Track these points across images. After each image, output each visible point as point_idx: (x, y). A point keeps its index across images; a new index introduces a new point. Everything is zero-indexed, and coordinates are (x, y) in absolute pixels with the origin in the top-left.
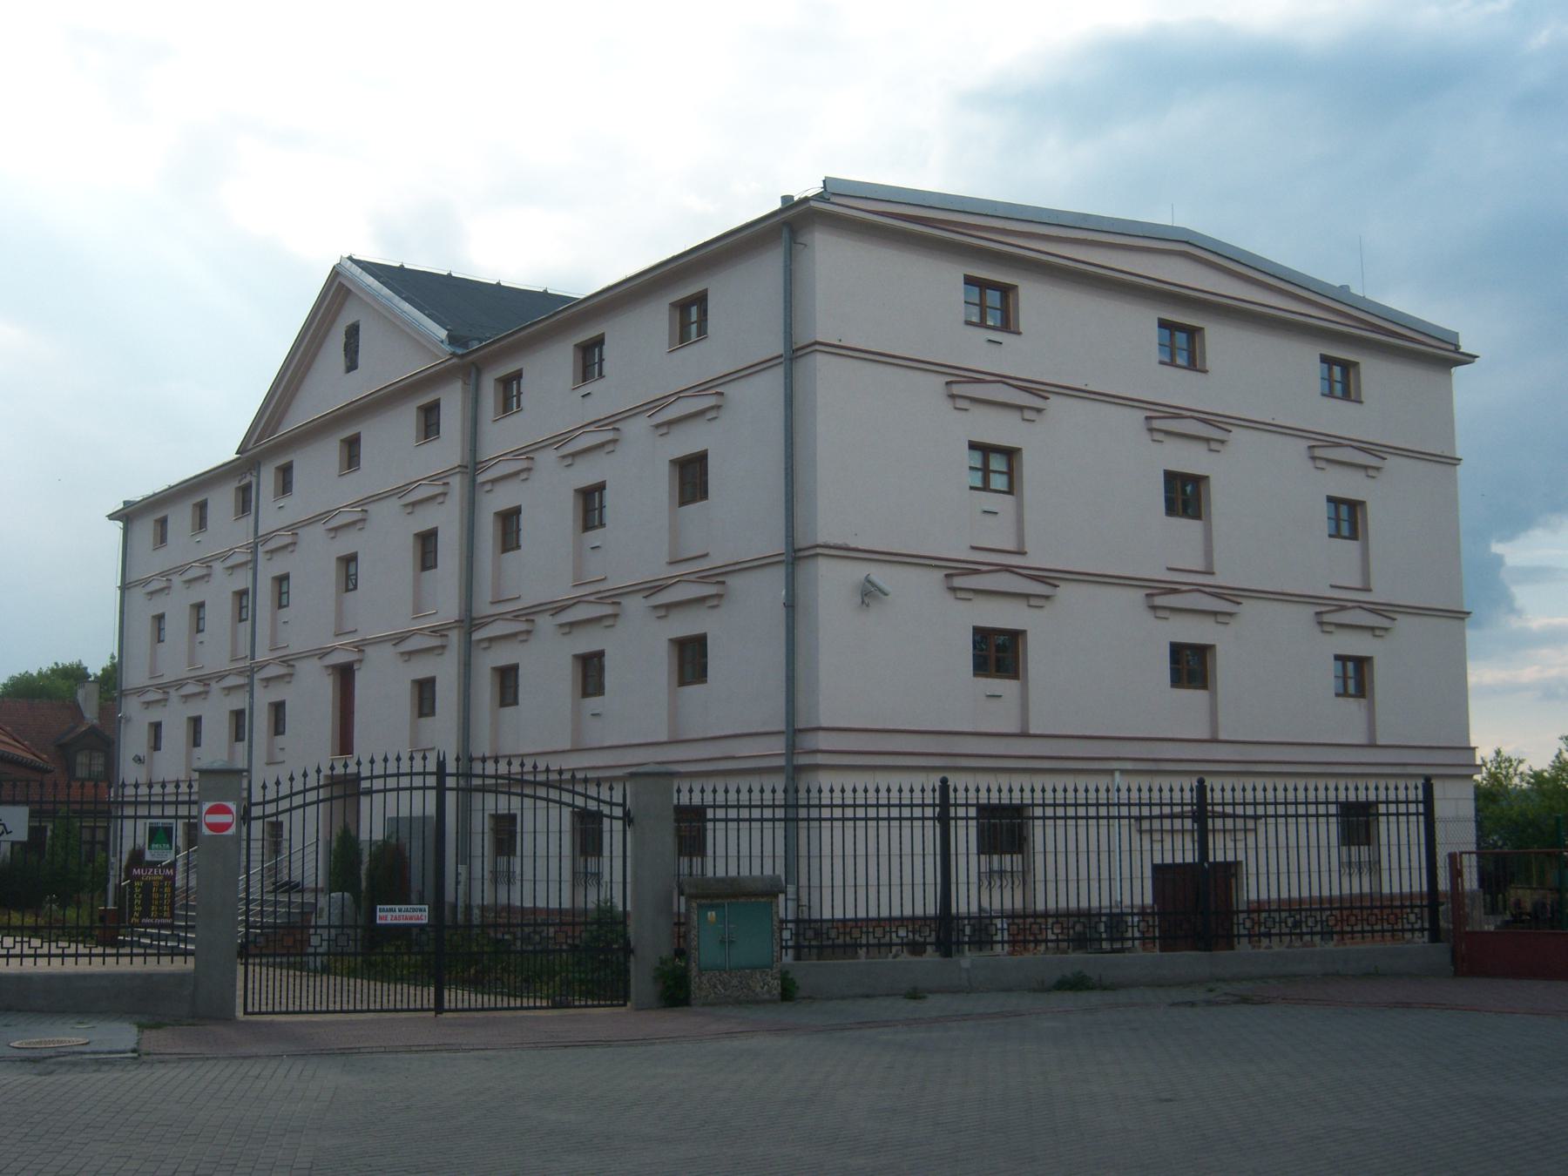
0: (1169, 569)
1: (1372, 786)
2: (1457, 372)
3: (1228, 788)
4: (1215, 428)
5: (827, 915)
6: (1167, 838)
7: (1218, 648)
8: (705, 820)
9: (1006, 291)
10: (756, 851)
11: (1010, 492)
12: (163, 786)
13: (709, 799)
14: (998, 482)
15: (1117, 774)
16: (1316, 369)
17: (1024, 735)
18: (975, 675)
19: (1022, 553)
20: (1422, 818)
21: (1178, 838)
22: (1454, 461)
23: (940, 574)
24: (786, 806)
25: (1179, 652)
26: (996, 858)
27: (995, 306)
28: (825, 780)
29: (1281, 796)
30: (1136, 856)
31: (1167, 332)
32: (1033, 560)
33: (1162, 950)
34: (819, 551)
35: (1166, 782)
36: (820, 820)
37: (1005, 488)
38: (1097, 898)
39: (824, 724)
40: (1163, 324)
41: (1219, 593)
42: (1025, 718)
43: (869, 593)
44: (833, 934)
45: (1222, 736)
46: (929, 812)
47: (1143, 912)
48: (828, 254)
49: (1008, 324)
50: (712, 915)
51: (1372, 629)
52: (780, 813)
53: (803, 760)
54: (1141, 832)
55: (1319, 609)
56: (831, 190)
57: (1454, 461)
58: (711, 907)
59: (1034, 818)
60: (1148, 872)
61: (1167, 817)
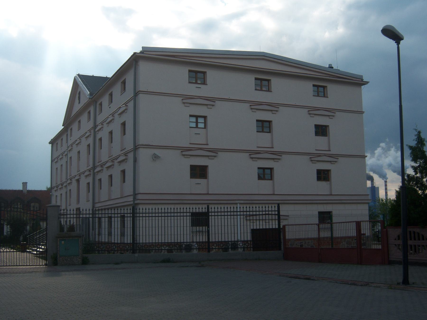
0: (190, 144)
1: (261, 207)
2: (363, 87)
3: (154, 209)
4: (274, 107)
5: (141, 242)
6: (271, 221)
7: (275, 169)
8: (209, 216)
9: (324, 87)
10: (147, 226)
11: (205, 128)
12: (64, 210)
13: (126, 212)
14: (201, 125)
15: (238, 204)
16: (311, 88)
17: (208, 194)
18: (191, 178)
19: (207, 144)
20: (131, 218)
21: (261, 222)
22: (362, 112)
23: (248, 154)
24: (76, 214)
25: (319, 172)
26: (198, 228)
27: (320, 91)
28: (141, 207)
29: (163, 211)
30: (245, 226)
31: (316, 88)
32: (211, 146)
33: (253, 251)
34: (139, 146)
35: (185, 206)
36: (237, 215)
37: (195, 126)
38: (231, 238)
39: (141, 192)
40: (314, 86)
41: (273, 153)
42: (274, 191)
43: (156, 157)
44: (127, 247)
45: (276, 193)
46: (138, 215)
47: (250, 241)
48: (143, 66)
49: (325, 96)
50: (63, 242)
51: (331, 162)
52: (75, 216)
53: (136, 202)
54: (247, 220)
55: (311, 156)
56: (145, 50)
57: (362, 112)
58: (63, 240)
59: (137, 217)
60: (249, 231)
61: (267, 214)
